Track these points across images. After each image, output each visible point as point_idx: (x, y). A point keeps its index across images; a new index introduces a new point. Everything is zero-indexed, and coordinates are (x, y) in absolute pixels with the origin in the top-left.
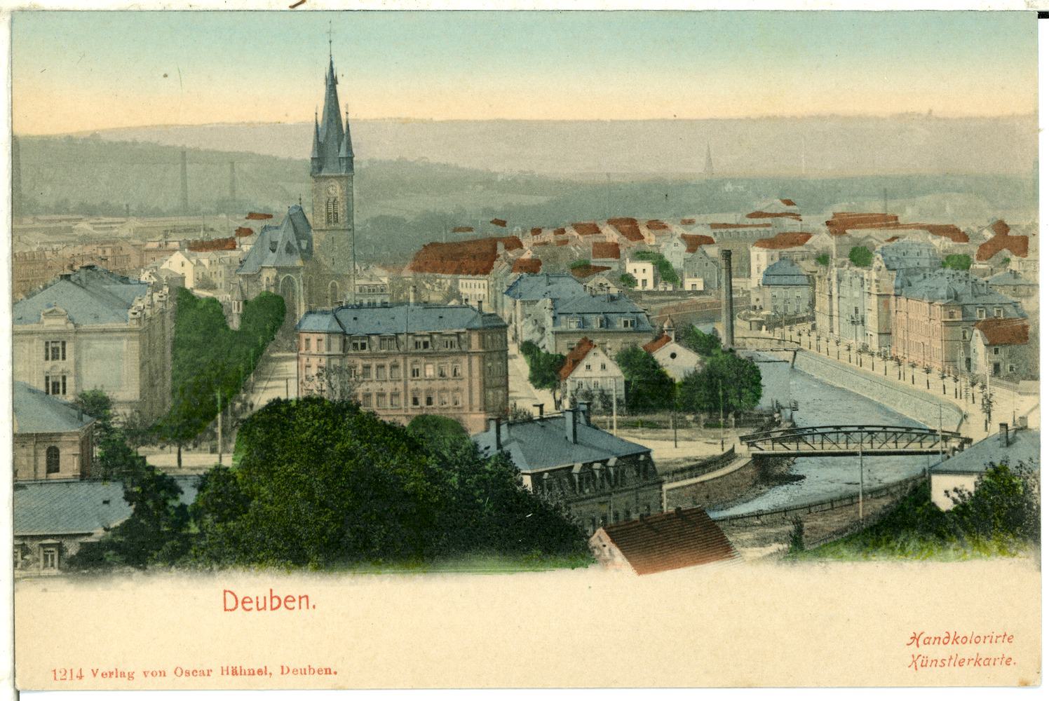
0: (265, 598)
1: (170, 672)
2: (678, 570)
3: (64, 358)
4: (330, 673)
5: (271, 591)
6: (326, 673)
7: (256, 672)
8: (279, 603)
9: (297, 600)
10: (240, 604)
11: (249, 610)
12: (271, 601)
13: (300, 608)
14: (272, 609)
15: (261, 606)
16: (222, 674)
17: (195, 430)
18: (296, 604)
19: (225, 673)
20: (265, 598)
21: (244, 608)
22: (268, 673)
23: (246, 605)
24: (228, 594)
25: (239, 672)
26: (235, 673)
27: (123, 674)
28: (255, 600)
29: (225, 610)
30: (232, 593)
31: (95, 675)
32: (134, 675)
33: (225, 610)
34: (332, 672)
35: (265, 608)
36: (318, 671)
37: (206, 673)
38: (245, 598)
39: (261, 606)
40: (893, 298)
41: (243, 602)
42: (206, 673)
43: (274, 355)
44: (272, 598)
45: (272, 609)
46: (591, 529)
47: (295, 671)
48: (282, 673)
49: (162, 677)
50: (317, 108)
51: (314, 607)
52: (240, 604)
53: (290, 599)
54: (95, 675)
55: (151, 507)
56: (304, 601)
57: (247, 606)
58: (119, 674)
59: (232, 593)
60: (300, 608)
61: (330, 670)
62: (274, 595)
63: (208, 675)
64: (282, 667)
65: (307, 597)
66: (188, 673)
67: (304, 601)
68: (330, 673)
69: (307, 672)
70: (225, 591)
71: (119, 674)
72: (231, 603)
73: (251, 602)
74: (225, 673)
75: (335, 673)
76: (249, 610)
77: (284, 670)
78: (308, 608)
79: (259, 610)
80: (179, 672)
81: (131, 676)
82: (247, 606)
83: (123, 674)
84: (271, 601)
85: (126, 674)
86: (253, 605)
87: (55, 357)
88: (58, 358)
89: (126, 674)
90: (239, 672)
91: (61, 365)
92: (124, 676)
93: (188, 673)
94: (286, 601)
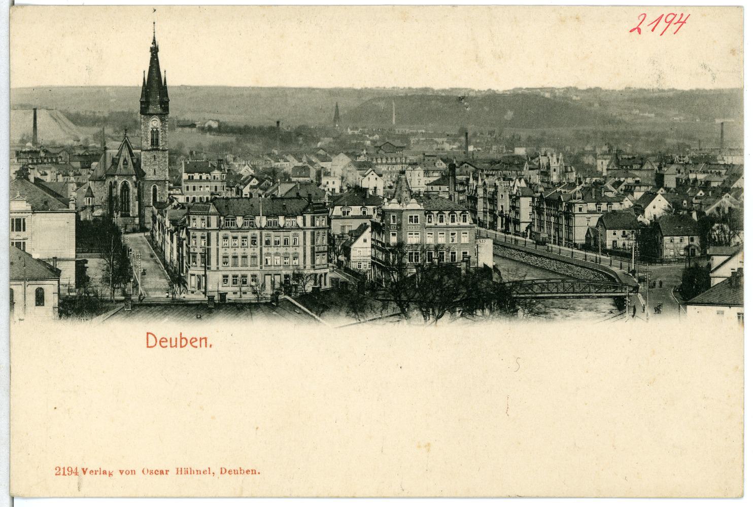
0: (176, 339)
1: (117, 475)
2: (128, 85)
3: (24, 230)
4: (255, 473)
5: (181, 334)
6: (252, 474)
7: (251, 472)
8: (182, 342)
9: (199, 339)
11: (166, 347)
12: (181, 342)
14: (181, 347)
15: (173, 344)
16: (177, 473)
19: (179, 472)
20: (176, 339)
21: (160, 344)
22: (211, 472)
24: (149, 335)
27: (105, 473)
29: (148, 347)
31: (122, 474)
32: (113, 474)
33: (148, 347)
34: (257, 472)
35: (176, 346)
36: (229, 471)
37: (165, 472)
38: (162, 339)
39: (173, 344)
40: (230, 246)
41: (160, 342)
42: (165, 472)
44: (181, 338)
45: (181, 347)
49: (133, 475)
51: (211, 346)
53: (194, 340)
54: (85, 472)
56: (203, 341)
57: (164, 344)
58: (102, 473)
61: (226, 470)
62: (183, 336)
63: (167, 474)
64: (178, 469)
65: (206, 338)
66: (151, 473)
67: (203, 341)
68: (255, 473)
70: (148, 333)
74: (179, 472)
75: (259, 473)
76: (166, 347)
77: (223, 471)
78: (206, 346)
79: (171, 347)
80: (145, 471)
81: (121, 472)
82: (164, 344)
83: (105, 473)
84: (181, 342)
85: (108, 473)
86: (168, 344)
87: (18, 229)
88: (20, 231)
89: (108, 473)
91: (22, 235)
92: (106, 474)
93: (151, 473)
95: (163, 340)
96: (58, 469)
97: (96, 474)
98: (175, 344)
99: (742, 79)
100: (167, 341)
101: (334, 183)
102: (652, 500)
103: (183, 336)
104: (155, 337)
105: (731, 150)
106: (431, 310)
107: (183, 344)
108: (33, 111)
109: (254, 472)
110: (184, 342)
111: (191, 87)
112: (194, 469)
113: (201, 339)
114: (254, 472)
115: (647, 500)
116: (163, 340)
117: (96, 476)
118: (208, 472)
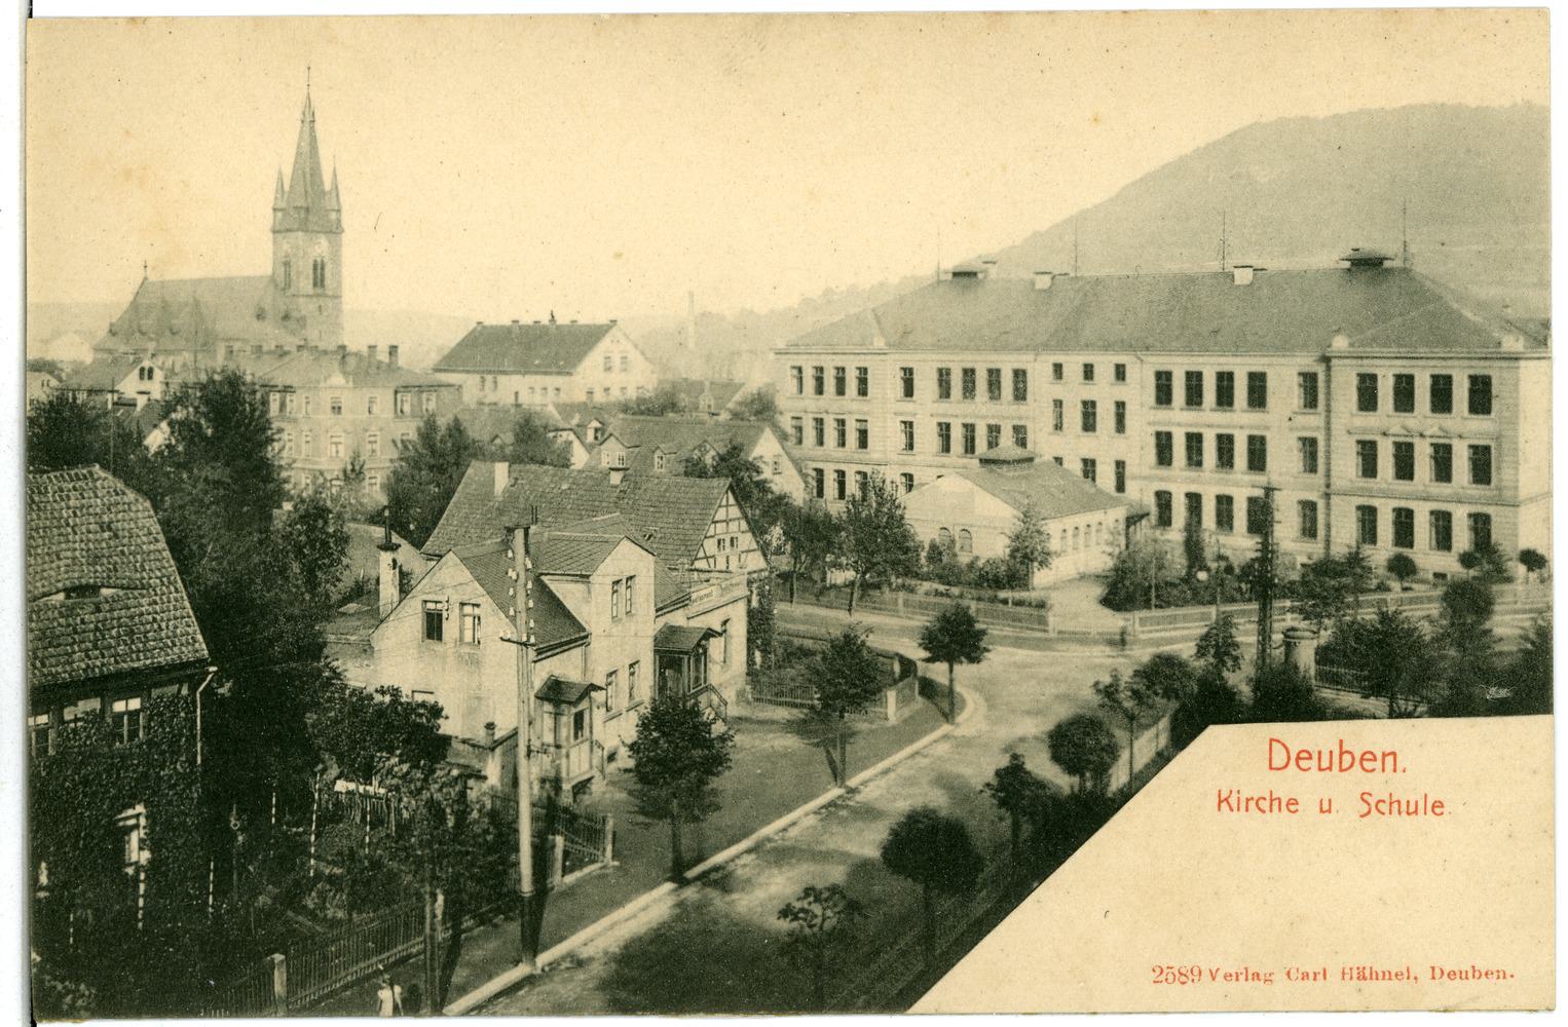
7: (1495, 975)
9: (1379, 757)
10: (1293, 762)
11: (1373, 770)
13: (1383, 770)
15: (1325, 764)
17: (1251, 582)
18: (1378, 764)
21: (1298, 766)
23: (1301, 763)
24: (1274, 744)
25: (1367, 974)
26: (1362, 977)
27: (1256, 976)
28: (1315, 756)
29: (1271, 768)
30: (1278, 741)
33: (1271, 768)
39: (1325, 764)
41: (1298, 758)
42: (1311, 976)
43: (44, 865)
46: (1121, 735)
47: (1451, 975)
48: (1433, 978)
50: (1104, 552)
52: (1293, 762)
53: (1304, 755)
54: (1214, 979)
55: (1476, 574)
58: (1250, 977)
59: (1278, 741)
60: (1383, 770)
61: (1258, 975)
62: (1345, 748)
64: (1433, 968)
65: (1394, 754)
67: (1389, 759)
69: (1470, 975)
70: (1271, 740)
71: (1250, 977)
72: (1279, 758)
73: (1310, 758)
76: (1373, 770)
79: (1320, 769)
82: (1303, 764)
83: (1256, 976)
86: (1314, 763)
89: (1262, 977)
90: (1367, 974)
94: (1362, 759)
95: (1367, 756)
96: (1158, 971)
97: (1237, 979)
98: (1328, 765)
99: (1549, 97)
100: (1375, 759)
101: (1120, 373)
102: (1108, 1016)
103: (1345, 748)
104: (1288, 752)
105: (1405, 260)
106: (1504, 693)
107: (1346, 764)
108: (34, 14)
109: (1501, 974)
110: (1347, 759)
111: (583, 15)
112: (1378, 968)
113: (1384, 755)
114: (1502, 975)
115: (1014, 1017)
116: (1367, 756)
117: (1351, 983)
118: (1406, 975)
